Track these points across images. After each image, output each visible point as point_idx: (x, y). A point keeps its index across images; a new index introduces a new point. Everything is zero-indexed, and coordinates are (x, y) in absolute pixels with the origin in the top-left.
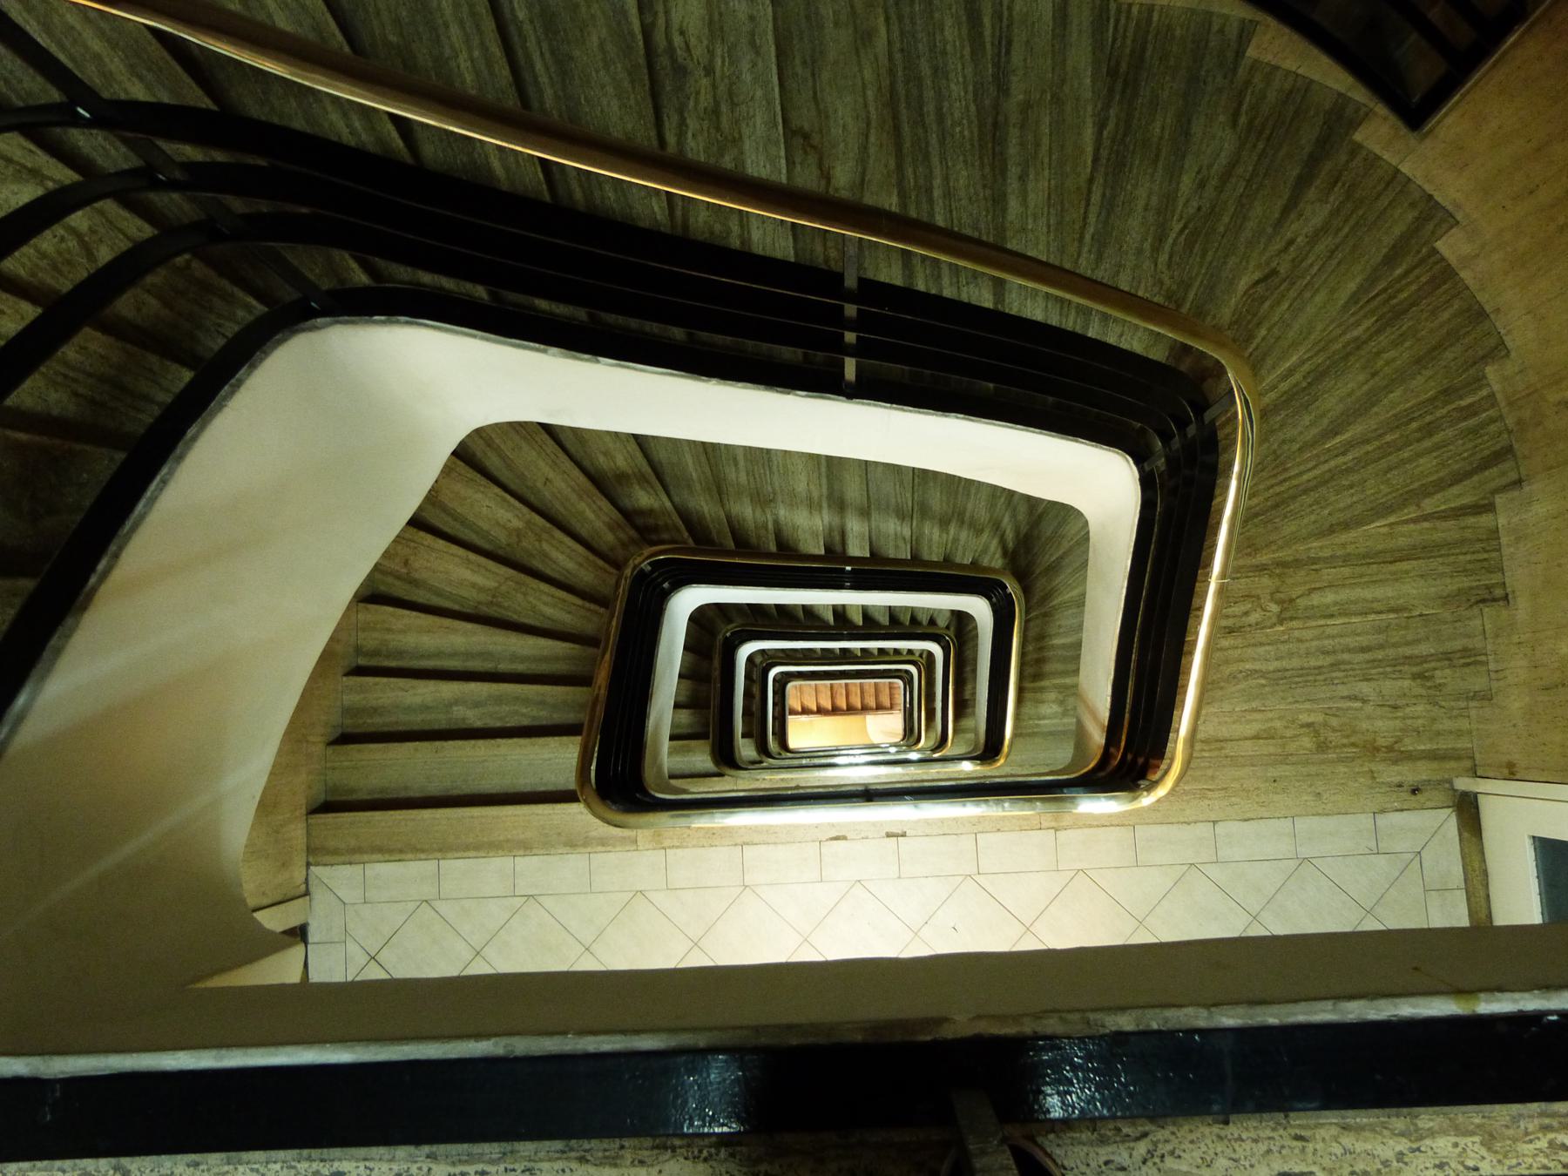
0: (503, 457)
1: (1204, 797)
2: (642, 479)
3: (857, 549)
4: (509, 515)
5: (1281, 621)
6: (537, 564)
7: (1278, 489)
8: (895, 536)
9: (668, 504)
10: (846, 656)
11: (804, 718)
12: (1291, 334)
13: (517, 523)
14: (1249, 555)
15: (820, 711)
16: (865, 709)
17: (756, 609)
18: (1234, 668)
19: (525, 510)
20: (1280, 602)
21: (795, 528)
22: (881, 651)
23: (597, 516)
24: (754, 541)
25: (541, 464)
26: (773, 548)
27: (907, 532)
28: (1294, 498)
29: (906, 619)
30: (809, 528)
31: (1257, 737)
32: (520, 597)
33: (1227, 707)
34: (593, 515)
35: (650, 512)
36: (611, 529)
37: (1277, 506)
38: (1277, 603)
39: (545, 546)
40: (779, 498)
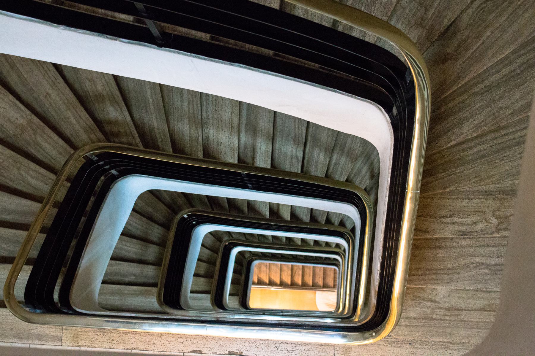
0: (20, 76)
1: (447, 348)
2: (113, 100)
3: (262, 161)
4: (18, 116)
5: (498, 231)
6: (32, 150)
7: (500, 140)
8: (290, 157)
9: (129, 118)
10: (290, 243)
11: (273, 289)
12: (506, 36)
13: (22, 121)
14: (475, 182)
15: (282, 284)
16: (315, 286)
17: (213, 201)
18: (468, 260)
19: (28, 112)
20: (499, 218)
21: (219, 144)
22: (316, 242)
23: (77, 121)
24: (187, 149)
25: (45, 83)
26: (200, 155)
27: (300, 154)
28: (510, 147)
29: (322, 219)
30: (228, 145)
31: (483, 309)
32: (15, 171)
33: (460, 286)
34: (75, 121)
35: (115, 123)
36: (86, 131)
37: (499, 151)
38: (497, 218)
39: (39, 139)
40: (210, 122)
